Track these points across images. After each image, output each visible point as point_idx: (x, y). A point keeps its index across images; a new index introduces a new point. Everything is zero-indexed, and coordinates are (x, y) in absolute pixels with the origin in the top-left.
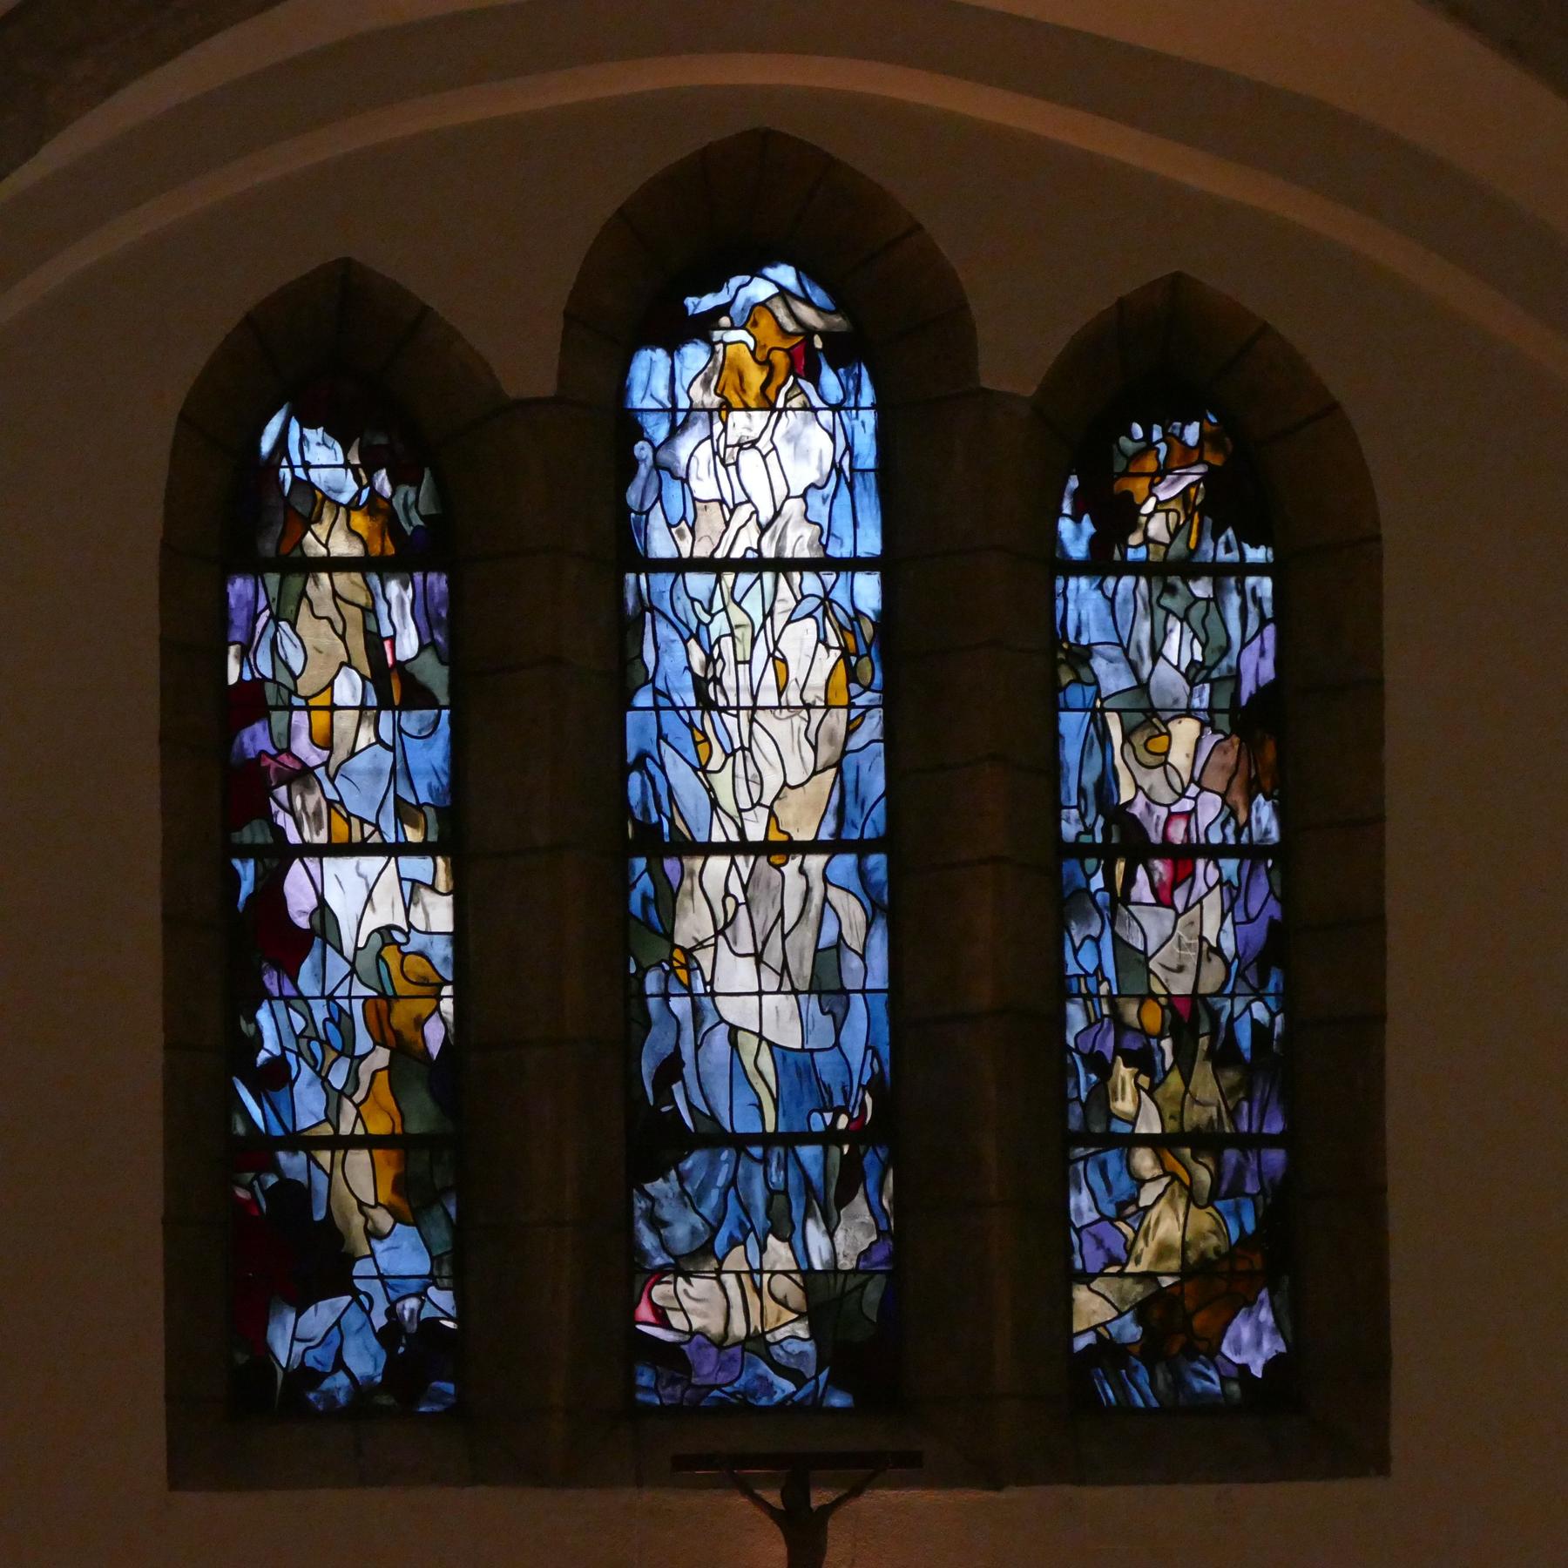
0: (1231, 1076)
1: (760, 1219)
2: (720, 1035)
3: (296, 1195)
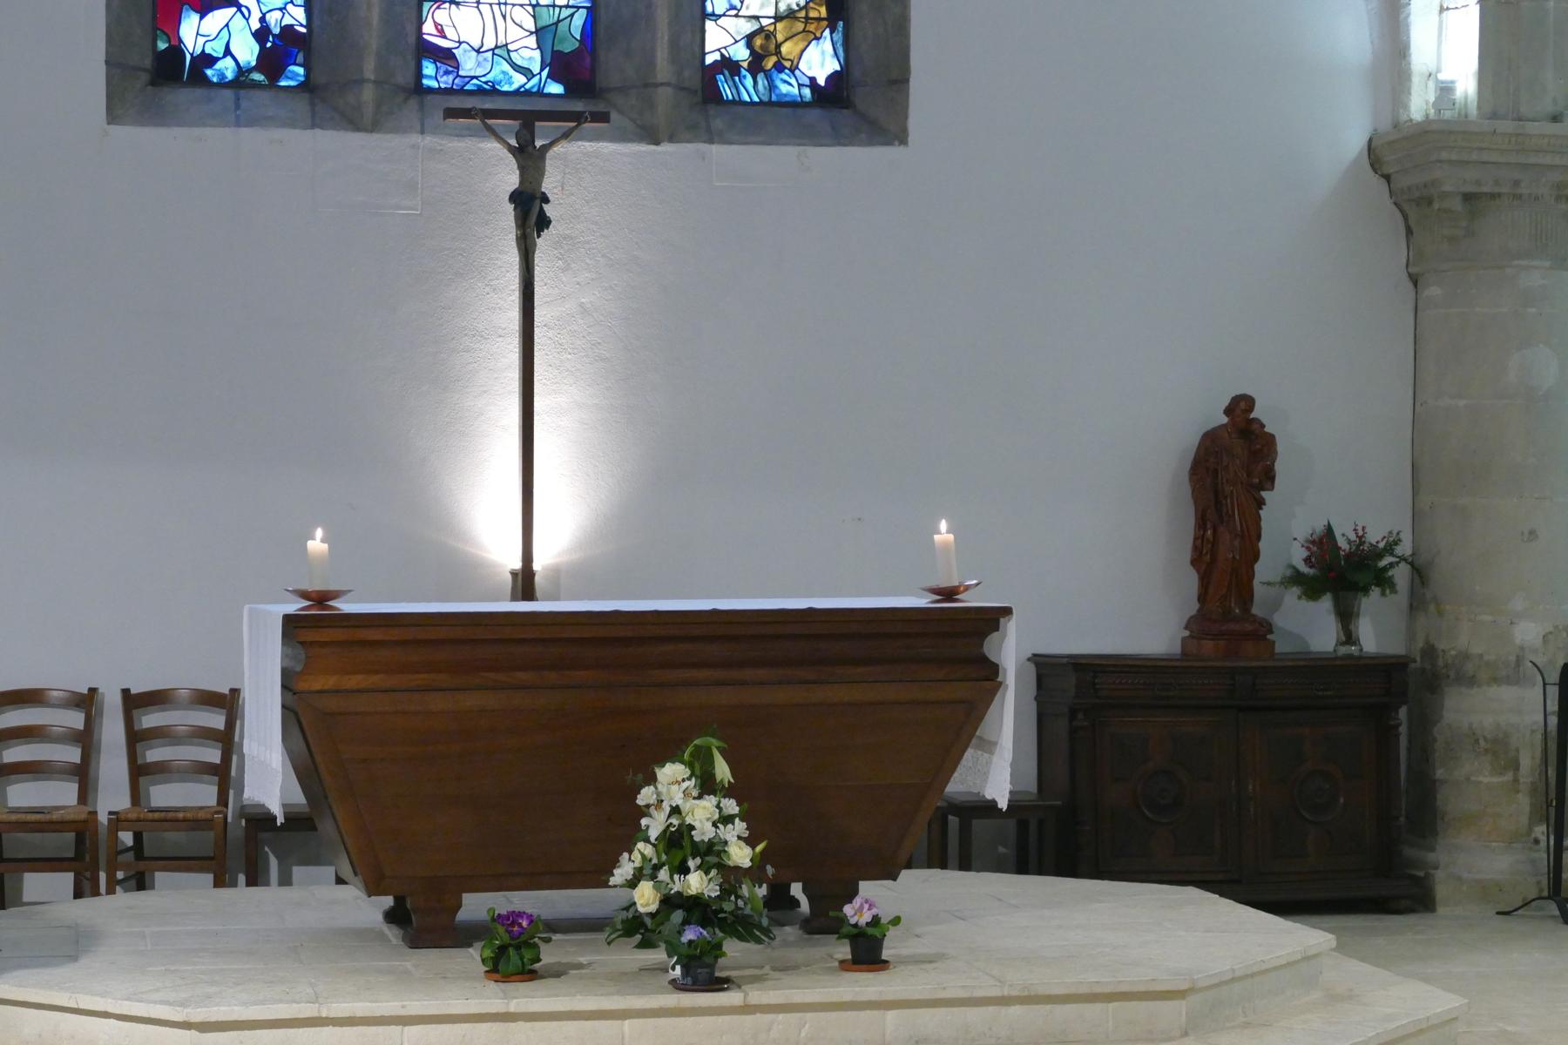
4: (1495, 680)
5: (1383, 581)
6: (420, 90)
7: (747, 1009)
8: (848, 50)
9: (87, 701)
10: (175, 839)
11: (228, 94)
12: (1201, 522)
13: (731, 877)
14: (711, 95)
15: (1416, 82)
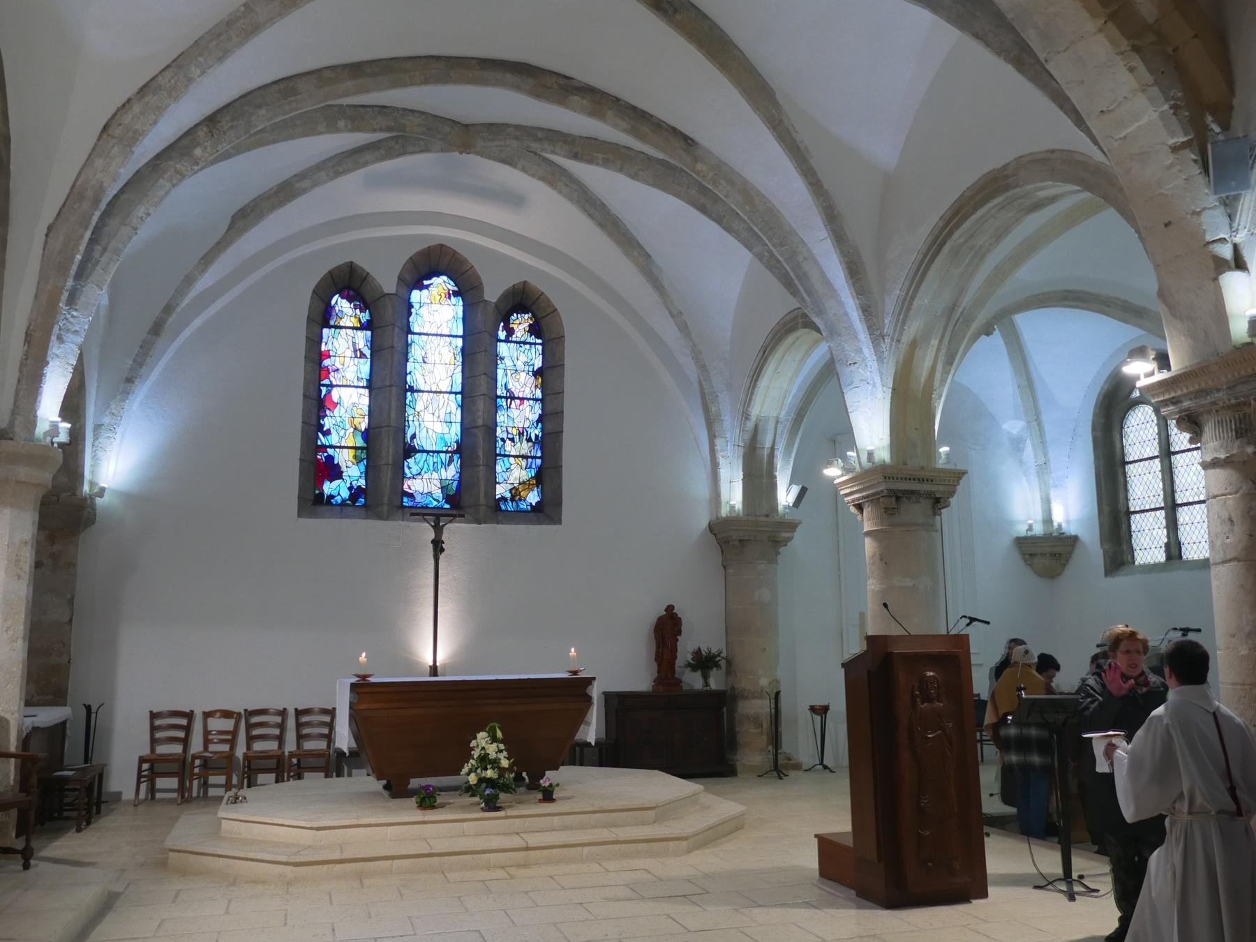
0: (530, 444)
1: (431, 468)
3: (330, 458)
4: (754, 698)
5: (717, 666)
7: (507, 817)
8: (543, 494)
9: (283, 713)
11: (339, 508)
12: (658, 647)
13: (502, 771)
15: (723, 504)
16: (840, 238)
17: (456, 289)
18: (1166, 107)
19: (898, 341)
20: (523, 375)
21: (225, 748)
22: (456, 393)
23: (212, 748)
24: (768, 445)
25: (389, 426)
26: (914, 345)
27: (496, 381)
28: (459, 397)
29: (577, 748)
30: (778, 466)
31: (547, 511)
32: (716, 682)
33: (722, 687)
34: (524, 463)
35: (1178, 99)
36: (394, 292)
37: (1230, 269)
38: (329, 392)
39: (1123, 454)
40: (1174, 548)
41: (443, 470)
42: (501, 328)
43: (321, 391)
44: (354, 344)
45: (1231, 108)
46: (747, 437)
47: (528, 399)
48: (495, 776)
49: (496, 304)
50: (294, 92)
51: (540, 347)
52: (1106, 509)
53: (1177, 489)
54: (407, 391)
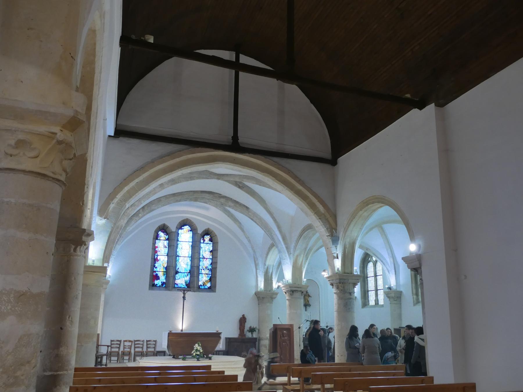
0: (209, 271)
1: (183, 277)
2: (181, 267)
3: (157, 274)
4: (265, 340)
5: (255, 331)
6: (175, 287)
7: (202, 362)
8: (211, 284)
9: (143, 341)
10: (149, 353)
11: (159, 287)
12: (240, 326)
13: (200, 353)
14: (199, 288)
15: (259, 287)
16: (280, 231)
17: (190, 229)
18: (325, 229)
19: (294, 255)
20: (207, 252)
21: (129, 350)
22: (190, 257)
23: (125, 350)
24: (271, 272)
25: (172, 266)
26: (297, 256)
27: (200, 254)
28: (190, 258)
29: (218, 352)
30: (273, 277)
31: (212, 289)
32: (255, 335)
33: (257, 337)
34: (207, 275)
35: (328, 227)
36: (175, 231)
37: (336, 258)
38: (157, 257)
39: (367, 275)
40: (377, 301)
41: (186, 278)
42: (202, 240)
43: (155, 257)
44: (164, 244)
45: (337, 229)
46: (265, 270)
47: (208, 259)
48: (199, 354)
49: (201, 234)
50: (160, 201)
51: (212, 245)
52: (363, 290)
53: (378, 285)
54: (177, 256)
